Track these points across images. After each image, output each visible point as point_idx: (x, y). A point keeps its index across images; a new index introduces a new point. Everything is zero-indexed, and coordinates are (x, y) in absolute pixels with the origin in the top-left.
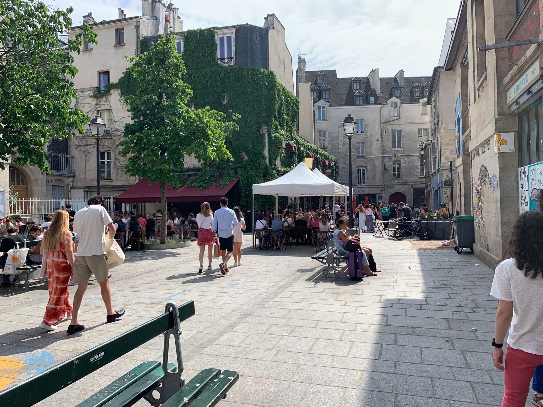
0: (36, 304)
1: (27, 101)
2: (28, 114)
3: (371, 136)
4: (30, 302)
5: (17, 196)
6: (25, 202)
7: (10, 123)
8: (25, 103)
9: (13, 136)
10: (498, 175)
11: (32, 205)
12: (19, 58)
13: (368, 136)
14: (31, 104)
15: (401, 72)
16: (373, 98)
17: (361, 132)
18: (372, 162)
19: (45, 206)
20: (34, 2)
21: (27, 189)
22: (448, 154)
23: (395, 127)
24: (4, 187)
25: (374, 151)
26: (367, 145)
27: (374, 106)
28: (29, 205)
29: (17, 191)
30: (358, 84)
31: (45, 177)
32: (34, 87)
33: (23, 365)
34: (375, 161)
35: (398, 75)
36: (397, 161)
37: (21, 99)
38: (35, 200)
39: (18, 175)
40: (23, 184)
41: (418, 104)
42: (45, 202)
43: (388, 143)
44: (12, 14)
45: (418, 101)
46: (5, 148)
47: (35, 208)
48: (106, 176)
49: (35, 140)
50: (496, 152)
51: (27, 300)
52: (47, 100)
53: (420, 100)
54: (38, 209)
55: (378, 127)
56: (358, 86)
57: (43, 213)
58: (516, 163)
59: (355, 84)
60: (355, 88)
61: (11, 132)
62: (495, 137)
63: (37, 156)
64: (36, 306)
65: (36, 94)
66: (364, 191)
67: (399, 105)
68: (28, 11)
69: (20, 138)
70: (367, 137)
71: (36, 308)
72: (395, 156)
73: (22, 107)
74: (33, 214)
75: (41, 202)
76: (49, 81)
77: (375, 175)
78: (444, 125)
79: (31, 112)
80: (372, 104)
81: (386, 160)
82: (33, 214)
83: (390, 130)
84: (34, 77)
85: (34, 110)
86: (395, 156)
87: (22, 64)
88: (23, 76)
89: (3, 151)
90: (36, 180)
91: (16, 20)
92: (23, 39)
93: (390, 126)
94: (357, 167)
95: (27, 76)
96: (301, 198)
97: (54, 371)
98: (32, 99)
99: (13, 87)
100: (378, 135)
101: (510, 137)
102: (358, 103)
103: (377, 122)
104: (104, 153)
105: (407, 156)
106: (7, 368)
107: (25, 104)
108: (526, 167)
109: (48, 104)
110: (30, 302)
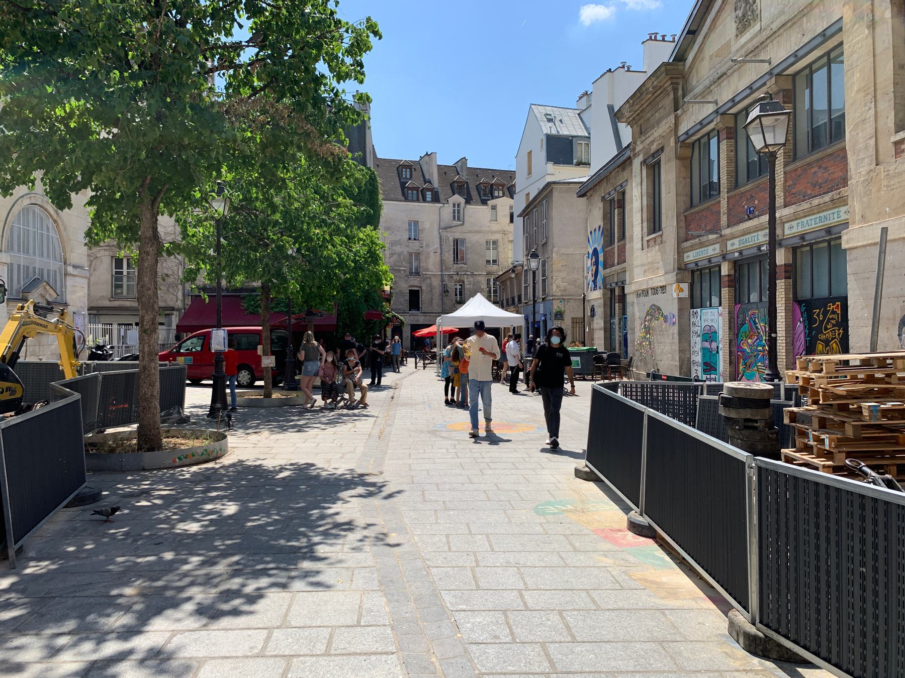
3: (427, 246)
10: (676, 312)
13: (424, 245)
15: (464, 160)
16: (430, 193)
17: (415, 239)
18: (428, 281)
22: (559, 282)
23: (458, 236)
25: (431, 267)
26: (422, 257)
27: (432, 205)
30: (408, 170)
34: (433, 279)
35: (460, 164)
36: (460, 281)
41: (486, 207)
43: (449, 256)
45: (486, 203)
48: (125, 293)
50: (675, 295)
53: (488, 202)
55: (436, 233)
56: (408, 173)
58: (689, 306)
59: (404, 170)
60: (404, 176)
62: (674, 286)
66: (418, 320)
67: (462, 205)
70: (422, 247)
72: (458, 274)
77: (432, 299)
78: (555, 249)
80: (429, 202)
81: (446, 278)
83: (451, 239)
86: (458, 274)
93: (452, 234)
94: (410, 286)
97: (559, 422)
100: (437, 245)
101: (685, 286)
102: (410, 198)
103: (436, 227)
104: (122, 259)
105: (473, 275)
108: (699, 310)
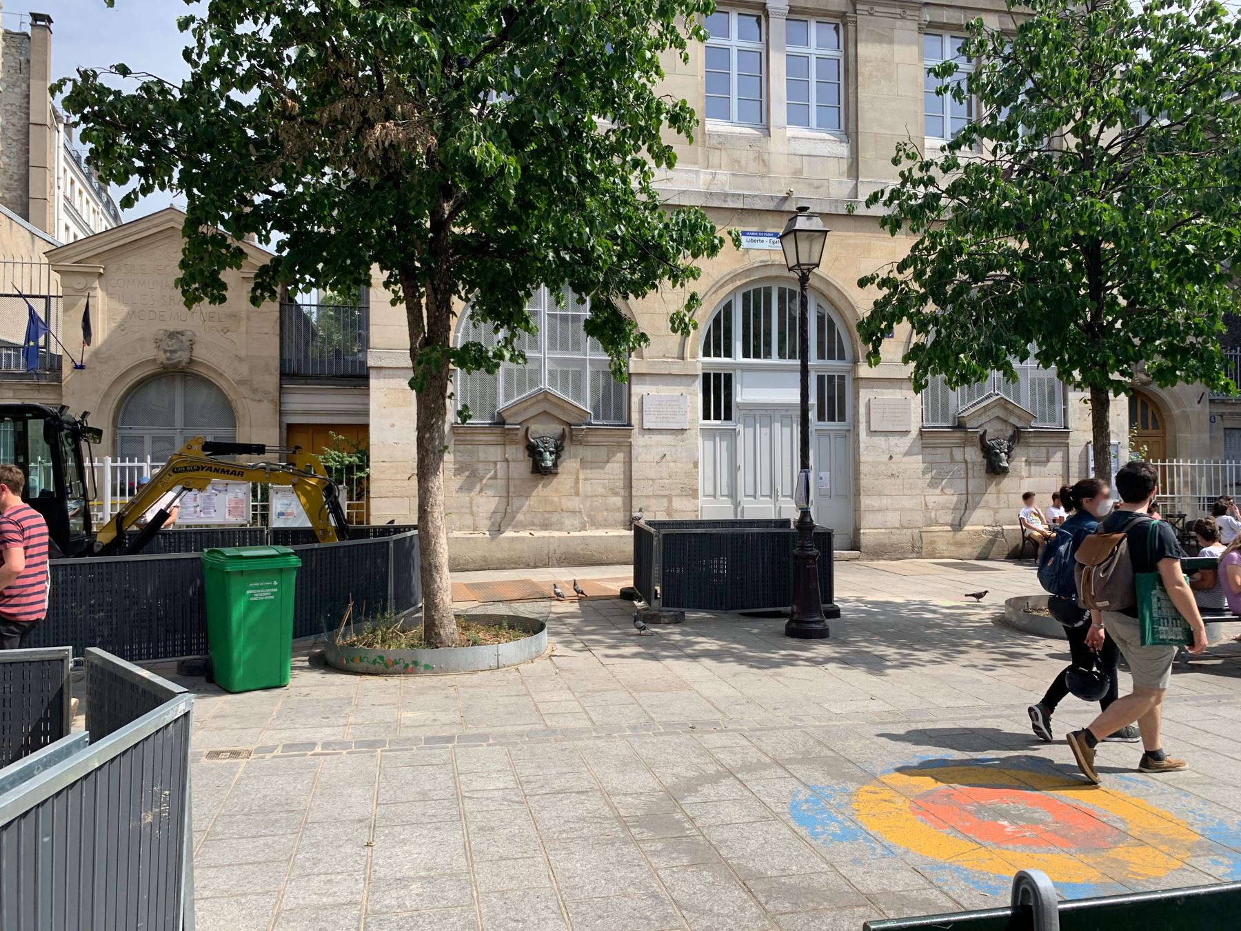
0: (1208, 705)
1: (1178, 238)
2: (1179, 269)
4: (1194, 698)
5: (1144, 455)
6: (1163, 467)
7: (1139, 295)
8: (1173, 244)
9: (1146, 320)
11: (1178, 475)
12: (1159, 145)
14: (1188, 243)
19: (1209, 476)
20: (1193, 5)
21: (1164, 438)
24: (1118, 435)
28: (1172, 476)
29: (1147, 443)
31: (1207, 411)
32: (1196, 201)
33: (1198, 838)
37: (1164, 237)
38: (1183, 464)
39: (1144, 405)
40: (1156, 427)
42: (1209, 468)
44: (1144, 54)
46: (1130, 349)
47: (1186, 483)
49: (1196, 324)
51: (1187, 692)
52: (1226, 225)
54: (1193, 482)
57: (1204, 494)
61: (1141, 313)
63: (1201, 360)
64: (1210, 710)
65: (1198, 216)
68: (1182, 32)
69: (1161, 323)
71: (1210, 714)
73: (1168, 254)
74: (1176, 495)
75: (1201, 468)
76: (1233, 180)
79: (1187, 262)
82: (1176, 495)
84: (1195, 180)
85: (1194, 255)
87: (1166, 156)
88: (1167, 182)
89: (1126, 357)
90: (1186, 417)
91: (1153, 64)
92: (1169, 100)
95: (1176, 181)
96: (366, 427)
98: (1189, 232)
99: (1148, 212)
106: (1162, 832)
107: (1173, 244)
109: (1229, 235)
110: (1194, 698)
